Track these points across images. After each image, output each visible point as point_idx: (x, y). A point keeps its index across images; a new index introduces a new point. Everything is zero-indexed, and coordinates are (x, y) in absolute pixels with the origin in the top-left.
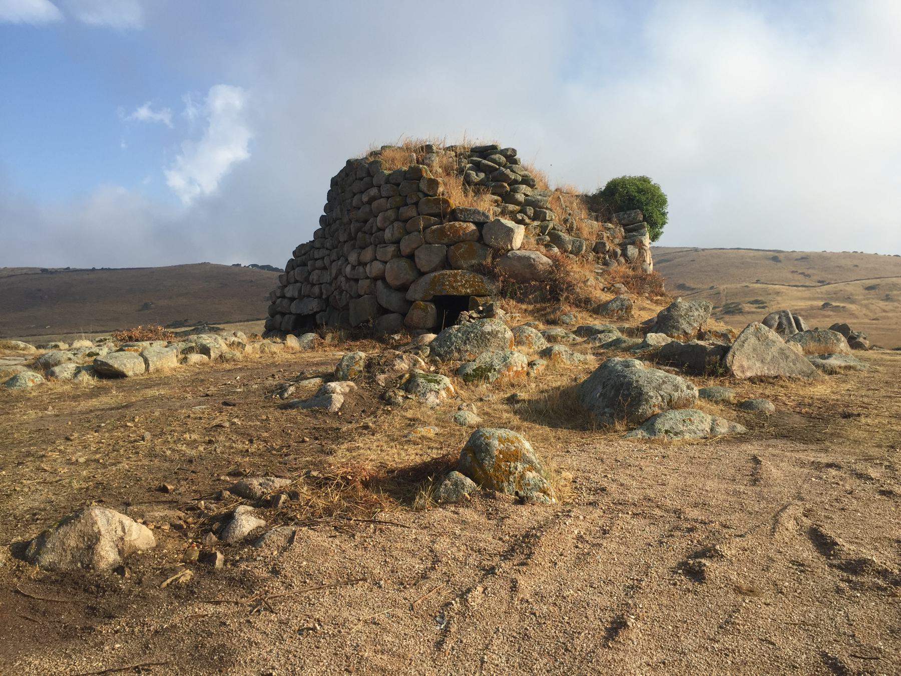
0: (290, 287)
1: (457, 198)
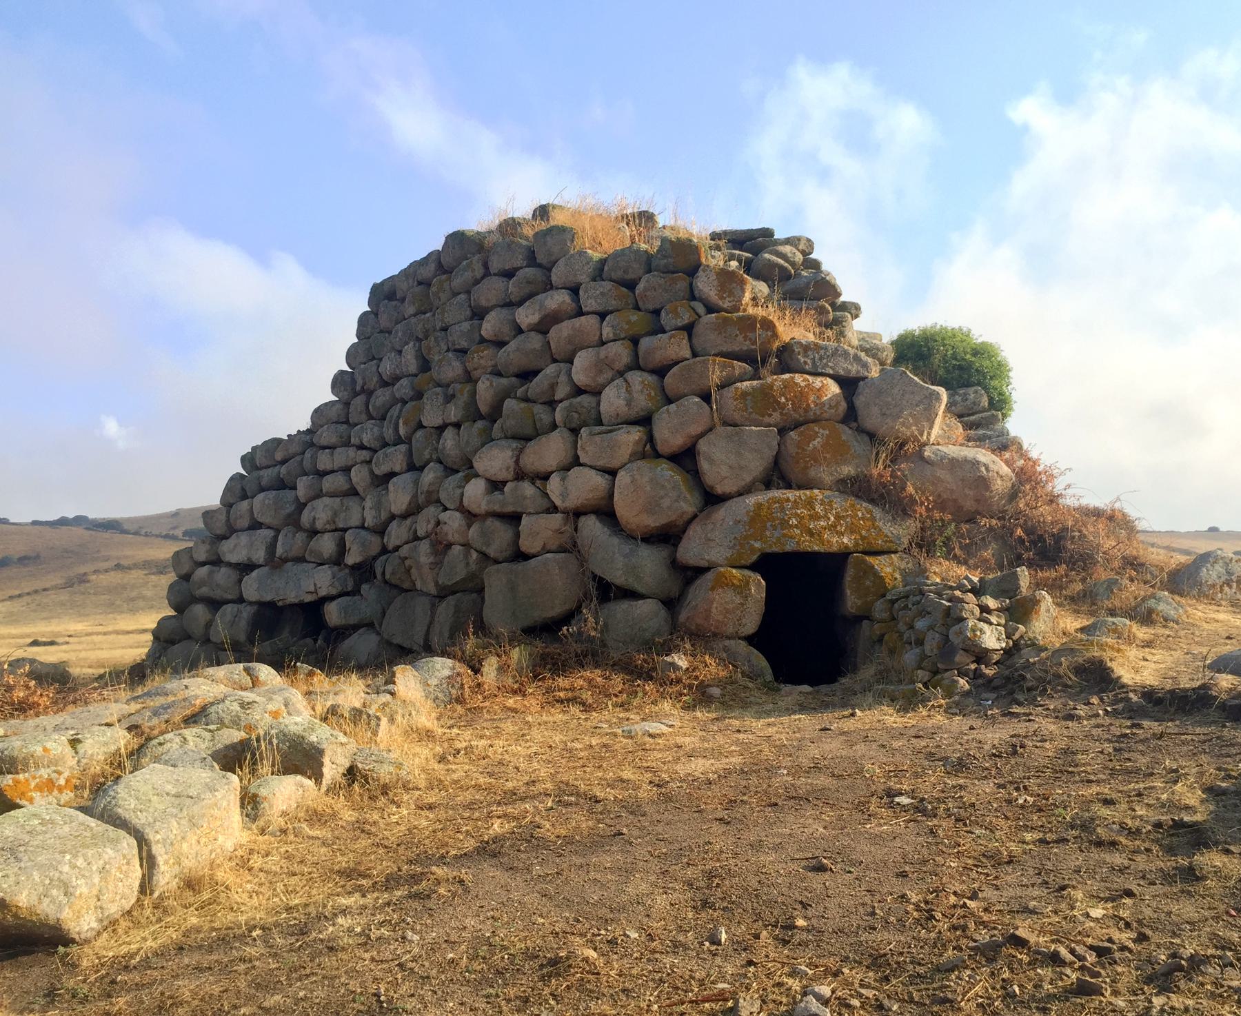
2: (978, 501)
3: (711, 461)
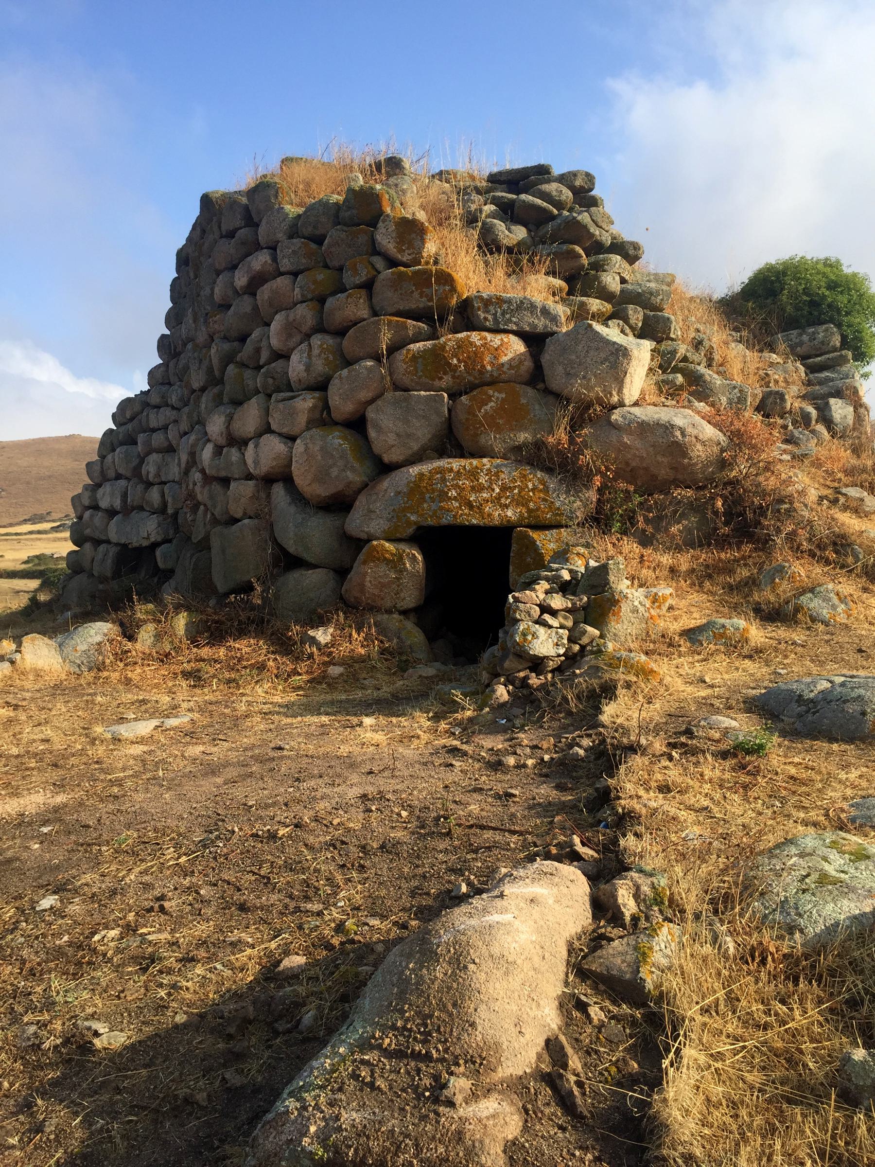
0: (107, 488)
1: (474, 277)
2: (675, 469)
3: (379, 429)
